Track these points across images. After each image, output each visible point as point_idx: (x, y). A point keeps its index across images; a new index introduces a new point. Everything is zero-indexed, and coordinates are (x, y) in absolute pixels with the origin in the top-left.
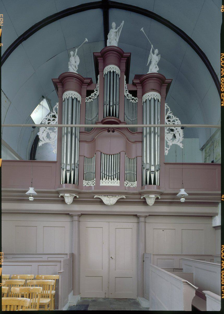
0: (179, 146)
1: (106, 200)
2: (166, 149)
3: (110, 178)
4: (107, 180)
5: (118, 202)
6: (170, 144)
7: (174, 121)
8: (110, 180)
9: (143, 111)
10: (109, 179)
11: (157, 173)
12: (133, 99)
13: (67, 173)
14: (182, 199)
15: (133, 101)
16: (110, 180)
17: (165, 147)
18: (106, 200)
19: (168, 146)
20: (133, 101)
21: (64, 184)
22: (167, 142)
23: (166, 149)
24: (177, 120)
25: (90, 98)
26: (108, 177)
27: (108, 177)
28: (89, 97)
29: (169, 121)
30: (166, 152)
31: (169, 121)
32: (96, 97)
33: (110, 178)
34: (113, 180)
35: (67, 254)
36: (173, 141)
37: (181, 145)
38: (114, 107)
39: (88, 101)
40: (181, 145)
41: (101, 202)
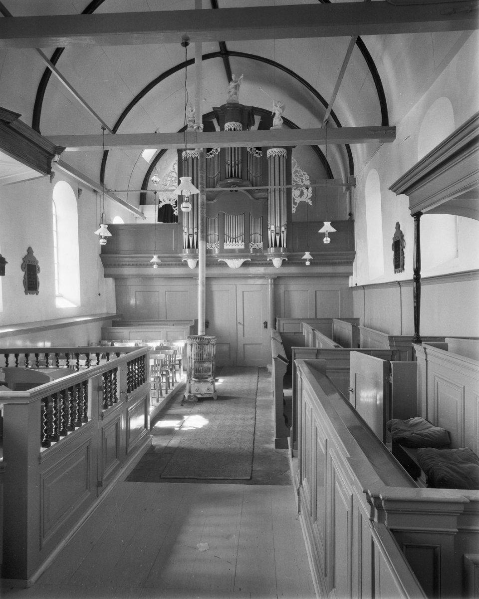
0: (307, 203)
1: (230, 262)
2: (293, 207)
3: (234, 240)
4: (237, 243)
5: (245, 265)
6: (298, 200)
7: (301, 176)
8: (234, 242)
9: (242, 276)
10: (233, 241)
11: (282, 235)
12: (257, 153)
13: (277, 236)
14: (184, 206)
15: (257, 156)
16: (234, 242)
17: (293, 205)
18: (230, 262)
19: (295, 204)
20: (257, 156)
21: (187, 249)
22: (294, 199)
23: (293, 207)
24: (304, 174)
25: (211, 154)
26: (232, 240)
27: (232, 240)
28: (210, 152)
29: (296, 176)
30: (294, 210)
31: (296, 176)
32: (217, 153)
33: (234, 240)
34: (237, 243)
35: (192, 321)
36: (301, 197)
37: (310, 202)
38: (237, 167)
39: (209, 158)
40: (310, 202)
41: (224, 265)
